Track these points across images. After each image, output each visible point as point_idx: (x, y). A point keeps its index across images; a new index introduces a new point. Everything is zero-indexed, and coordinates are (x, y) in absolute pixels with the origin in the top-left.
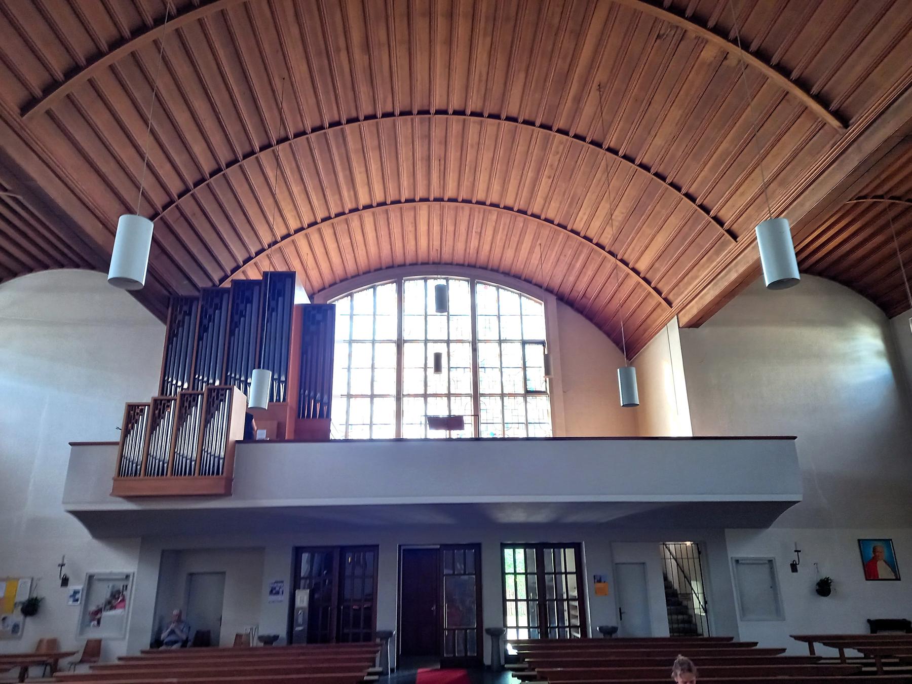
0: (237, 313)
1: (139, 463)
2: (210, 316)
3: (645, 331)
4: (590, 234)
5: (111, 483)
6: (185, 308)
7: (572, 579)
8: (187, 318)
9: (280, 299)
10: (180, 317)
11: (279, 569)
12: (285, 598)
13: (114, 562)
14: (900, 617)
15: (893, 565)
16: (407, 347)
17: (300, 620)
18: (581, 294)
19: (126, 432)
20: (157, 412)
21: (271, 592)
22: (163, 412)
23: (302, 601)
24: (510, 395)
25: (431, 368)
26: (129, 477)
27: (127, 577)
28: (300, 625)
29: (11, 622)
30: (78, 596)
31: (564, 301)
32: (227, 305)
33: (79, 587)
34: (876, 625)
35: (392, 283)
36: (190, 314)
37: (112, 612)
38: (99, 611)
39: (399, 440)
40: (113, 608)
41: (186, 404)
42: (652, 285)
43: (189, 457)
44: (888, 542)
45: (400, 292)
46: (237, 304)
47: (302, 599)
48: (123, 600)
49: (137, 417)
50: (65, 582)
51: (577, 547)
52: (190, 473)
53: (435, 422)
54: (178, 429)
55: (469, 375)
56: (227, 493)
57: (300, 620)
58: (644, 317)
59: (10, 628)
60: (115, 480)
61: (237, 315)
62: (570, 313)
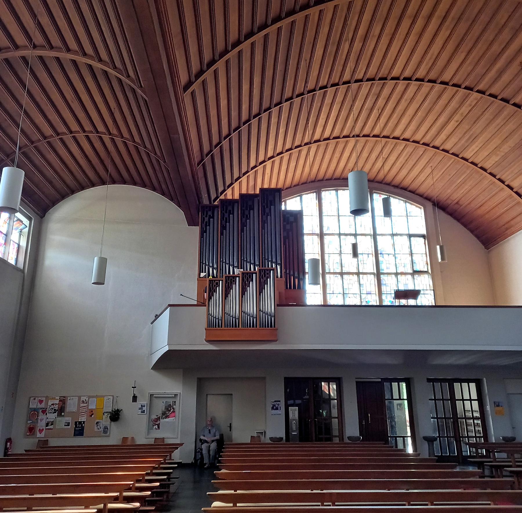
2: (226, 218)
3: (507, 229)
6: (210, 213)
7: (475, 404)
10: (206, 219)
11: (277, 392)
12: (282, 411)
13: (170, 386)
16: (326, 239)
17: (294, 428)
18: (456, 201)
21: (273, 408)
22: (231, 285)
23: (294, 414)
25: (364, 254)
26: (246, 328)
27: (176, 395)
28: (294, 431)
29: (102, 425)
30: (144, 408)
31: (438, 206)
33: (145, 403)
35: (313, 193)
36: (213, 217)
37: (167, 420)
38: (158, 419)
39: (325, 305)
40: (167, 417)
41: (246, 280)
43: (214, 316)
45: (319, 199)
46: (244, 210)
47: (294, 413)
48: (174, 412)
49: (214, 288)
50: (135, 399)
51: (409, 382)
53: (400, 294)
54: (242, 297)
55: (372, 259)
57: (294, 428)
59: (102, 430)
61: (245, 217)
62: (443, 215)
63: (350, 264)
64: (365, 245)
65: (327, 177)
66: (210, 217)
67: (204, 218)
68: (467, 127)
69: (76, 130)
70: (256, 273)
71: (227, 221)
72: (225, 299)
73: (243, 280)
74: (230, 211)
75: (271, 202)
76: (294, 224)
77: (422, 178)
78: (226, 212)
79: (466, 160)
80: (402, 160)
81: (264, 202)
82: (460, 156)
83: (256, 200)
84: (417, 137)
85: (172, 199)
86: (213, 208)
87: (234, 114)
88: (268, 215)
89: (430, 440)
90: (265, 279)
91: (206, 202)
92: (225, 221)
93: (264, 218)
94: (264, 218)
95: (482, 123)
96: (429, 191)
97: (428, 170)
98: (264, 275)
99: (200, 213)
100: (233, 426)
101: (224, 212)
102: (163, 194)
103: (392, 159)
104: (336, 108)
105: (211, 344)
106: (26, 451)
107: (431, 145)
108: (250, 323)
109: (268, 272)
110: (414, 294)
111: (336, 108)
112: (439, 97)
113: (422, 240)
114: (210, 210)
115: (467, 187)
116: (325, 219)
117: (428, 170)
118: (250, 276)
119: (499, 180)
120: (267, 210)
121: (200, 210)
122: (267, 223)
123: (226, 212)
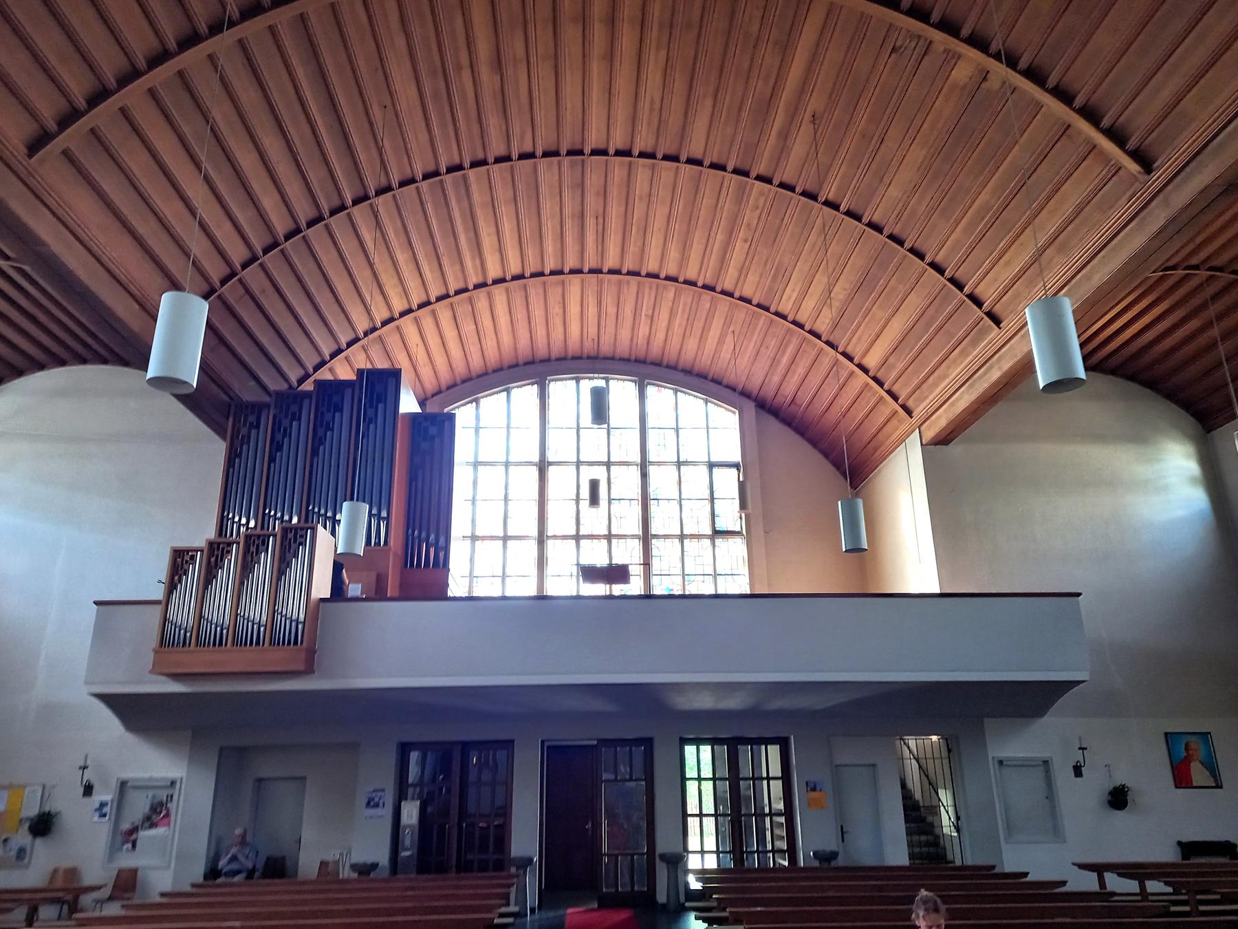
0: (321, 426)
1: (189, 628)
2: (285, 429)
3: (876, 449)
4: (801, 318)
5: (151, 656)
6: (252, 419)
7: (777, 787)
8: (254, 432)
9: (381, 406)
10: (244, 431)
11: (378, 773)
12: (387, 812)
13: (154, 763)
14: (1222, 838)
15: (1212, 767)
16: (552, 471)
17: (408, 842)
18: (789, 399)
19: (172, 587)
20: (213, 559)
21: (368, 804)
22: (222, 560)
23: (410, 816)
25: (585, 500)
27: (173, 783)
28: (407, 849)
29: (14, 845)
30: (107, 809)
31: (765, 409)
32: (308, 414)
33: (107, 798)
34: (1189, 849)
35: (532, 384)
36: (258, 427)
37: (153, 832)
38: (134, 830)
39: (541, 598)
40: (153, 825)
41: (253, 549)
42: (886, 387)
43: (257, 620)
44: (1205, 736)
45: (543, 396)
46: (322, 413)
47: (411, 813)
48: (167, 815)
49: (185, 566)
50: (88, 790)
51: (783, 743)
52: (258, 643)
53: (590, 573)
54: (242, 583)
55: (637, 509)
56: (309, 669)
57: (408, 842)
58: (874, 430)
59: (13, 853)
60: (156, 652)
61: (322, 428)
62: (773, 425)
64: (626, 482)
89: (126, 883)
106: (194, 886)
110: (617, 573)
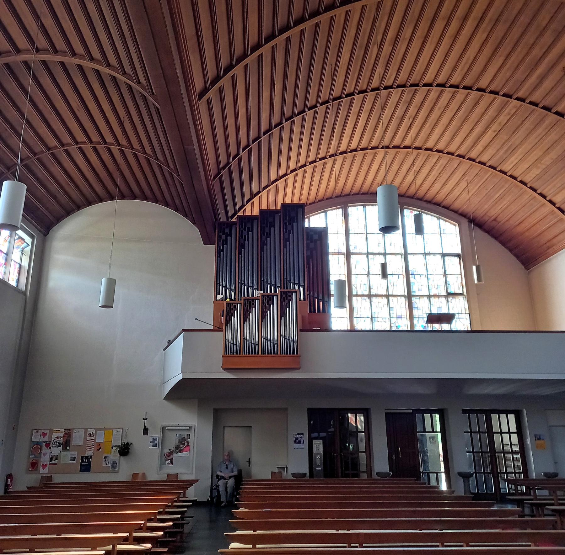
2: (245, 236)
3: (549, 248)
6: (227, 231)
7: (515, 437)
10: (223, 237)
11: (300, 424)
12: (306, 445)
13: (184, 418)
16: (353, 258)
17: (318, 463)
18: (493, 218)
21: (295, 442)
22: (250, 309)
23: (318, 448)
24: (381, 296)
25: (394, 275)
26: (267, 355)
27: (190, 428)
28: (318, 467)
29: (110, 460)
30: (156, 442)
31: (474, 223)
33: (156, 436)
35: (339, 208)
36: (231, 235)
37: (181, 454)
38: (171, 453)
39: (352, 330)
40: (181, 451)
41: (266, 303)
43: (232, 342)
45: (346, 215)
46: (264, 227)
47: (318, 446)
48: (188, 445)
49: (232, 311)
50: (146, 431)
51: (442, 413)
53: (432, 318)
54: (262, 321)
55: (403, 280)
57: (318, 463)
59: (110, 465)
61: (265, 234)
62: (479, 233)
63: (379, 286)
64: (395, 265)
65: (354, 191)
66: (227, 235)
67: (221, 236)
68: (506, 138)
69: (82, 141)
70: (277, 296)
71: (246, 239)
72: (244, 323)
73: (263, 302)
74: (249, 228)
75: (293, 218)
76: (318, 242)
77: (456, 193)
78: (245, 230)
79: (505, 173)
80: (435, 173)
81: (286, 219)
82: (498, 169)
83: (277, 217)
84: (452, 149)
85: (186, 216)
86: (231, 225)
87: (254, 123)
88: (290, 233)
90: (287, 301)
91: (223, 218)
92: (243, 239)
93: (286, 236)
94: (286, 236)
95: (521, 133)
96: (464, 207)
97: (463, 184)
98: (285, 298)
99: (217, 230)
100: (253, 460)
101: (242, 229)
102: (177, 210)
103: (425, 172)
104: (363, 116)
105: (229, 372)
106: (28, 488)
107: (467, 157)
108: (271, 350)
109: (290, 294)
111: (363, 116)
112: (476, 105)
113: (456, 259)
114: (227, 227)
115: (505, 202)
116: (351, 237)
117: (463, 184)
118: (270, 298)
119: (541, 194)
120: (289, 227)
121: (217, 227)
122: (289, 241)
123: (245, 230)
